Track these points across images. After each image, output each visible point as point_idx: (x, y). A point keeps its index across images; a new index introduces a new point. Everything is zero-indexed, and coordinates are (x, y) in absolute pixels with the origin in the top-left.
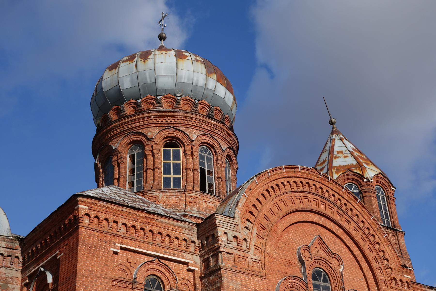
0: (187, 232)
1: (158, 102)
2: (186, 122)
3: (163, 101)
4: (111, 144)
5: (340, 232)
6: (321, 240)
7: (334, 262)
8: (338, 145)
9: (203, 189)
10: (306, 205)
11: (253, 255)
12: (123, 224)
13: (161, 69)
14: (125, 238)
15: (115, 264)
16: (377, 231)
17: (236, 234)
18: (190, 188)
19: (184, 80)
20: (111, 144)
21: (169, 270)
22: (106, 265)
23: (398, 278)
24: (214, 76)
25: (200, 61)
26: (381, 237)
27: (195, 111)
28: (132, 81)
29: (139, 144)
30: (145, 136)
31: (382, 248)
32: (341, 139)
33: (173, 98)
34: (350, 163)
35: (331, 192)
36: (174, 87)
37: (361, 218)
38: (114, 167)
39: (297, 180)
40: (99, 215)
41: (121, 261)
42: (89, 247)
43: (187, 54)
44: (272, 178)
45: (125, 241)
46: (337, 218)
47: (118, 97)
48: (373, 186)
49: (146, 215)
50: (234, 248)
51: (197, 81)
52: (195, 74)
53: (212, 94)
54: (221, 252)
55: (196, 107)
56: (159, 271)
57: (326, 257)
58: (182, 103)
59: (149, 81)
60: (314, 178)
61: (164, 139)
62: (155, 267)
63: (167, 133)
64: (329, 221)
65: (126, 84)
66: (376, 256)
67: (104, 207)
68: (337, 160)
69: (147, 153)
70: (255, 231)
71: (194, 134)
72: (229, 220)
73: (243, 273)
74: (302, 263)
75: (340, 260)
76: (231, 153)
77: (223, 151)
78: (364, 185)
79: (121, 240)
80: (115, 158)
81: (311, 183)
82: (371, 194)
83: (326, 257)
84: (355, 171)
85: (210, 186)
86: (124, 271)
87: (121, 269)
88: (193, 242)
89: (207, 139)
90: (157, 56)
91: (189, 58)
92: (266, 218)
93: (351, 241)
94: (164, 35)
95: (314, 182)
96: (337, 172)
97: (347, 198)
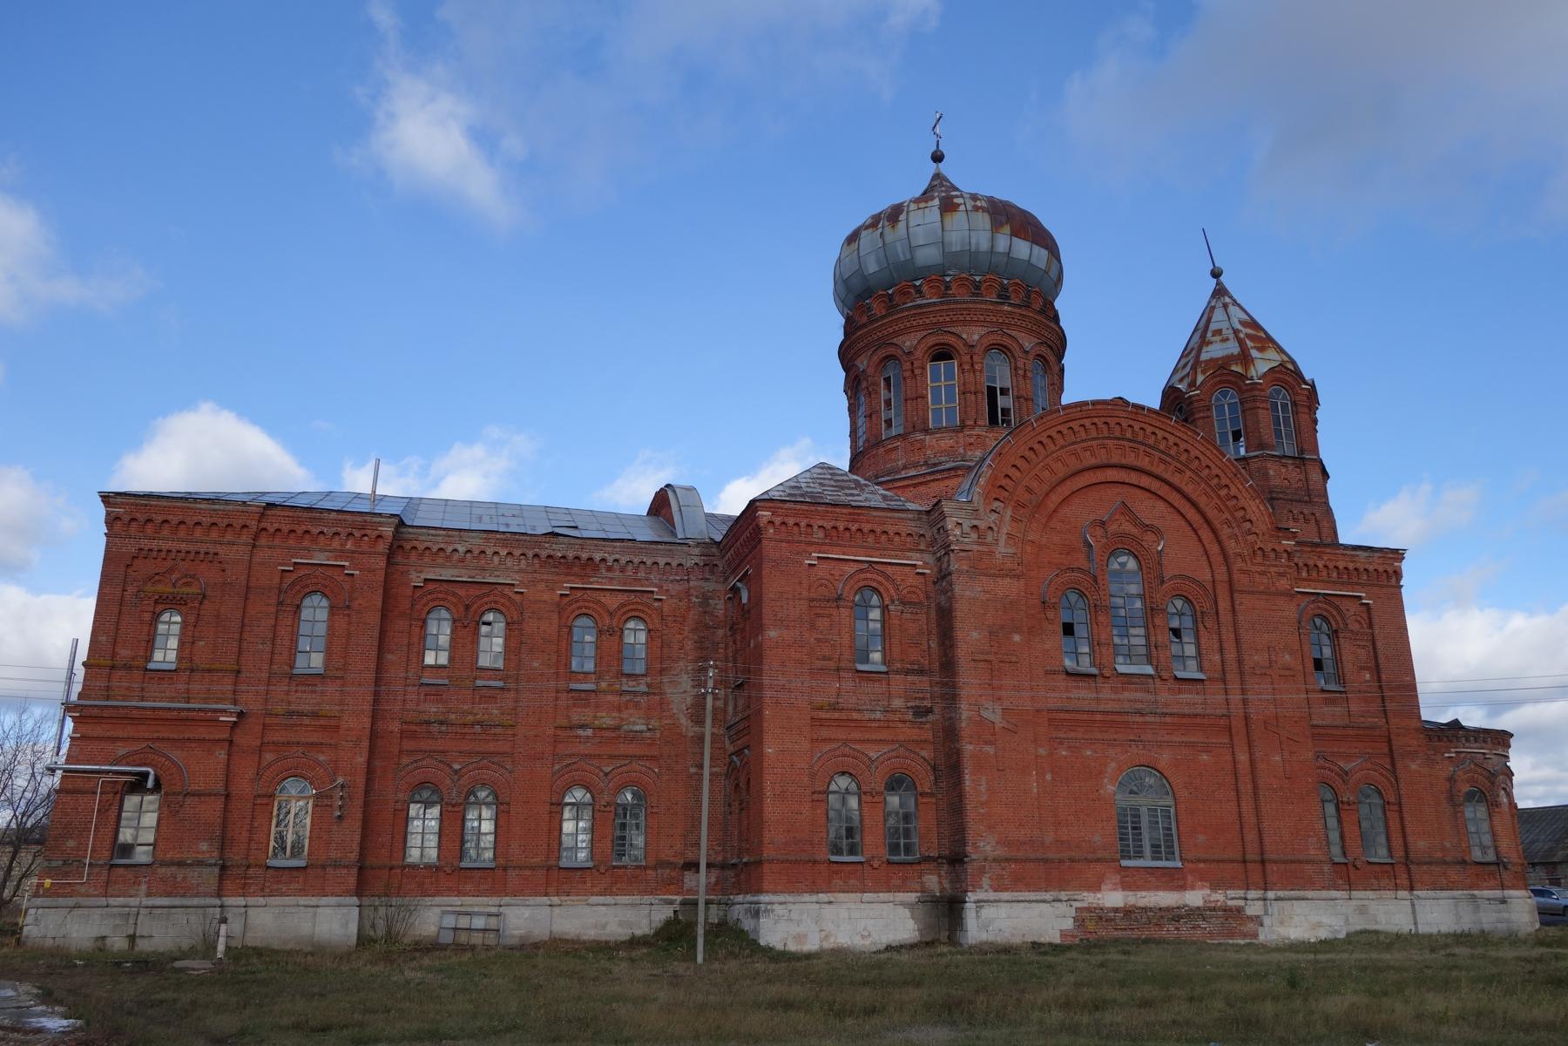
4: (500, 664)
5: (1164, 490)
6: (1125, 508)
7: (1150, 537)
9: (993, 420)
10: (1103, 458)
11: (1003, 549)
13: (919, 237)
17: (975, 522)
18: (971, 423)
19: (956, 248)
20: (500, 664)
21: (887, 577)
23: (1268, 548)
24: (1007, 229)
33: (936, 277)
34: (1229, 352)
35: (1149, 429)
37: (1205, 462)
39: (1087, 422)
46: (1159, 470)
51: (978, 244)
55: (978, 288)
57: (1134, 531)
63: (932, 340)
68: (1210, 348)
70: (1009, 513)
71: (974, 334)
75: (1158, 533)
76: (1044, 350)
77: (1027, 352)
81: (1112, 422)
83: (1134, 531)
84: (1234, 368)
85: (1005, 412)
91: (962, 208)
92: (1029, 490)
93: (1183, 501)
96: (1204, 372)
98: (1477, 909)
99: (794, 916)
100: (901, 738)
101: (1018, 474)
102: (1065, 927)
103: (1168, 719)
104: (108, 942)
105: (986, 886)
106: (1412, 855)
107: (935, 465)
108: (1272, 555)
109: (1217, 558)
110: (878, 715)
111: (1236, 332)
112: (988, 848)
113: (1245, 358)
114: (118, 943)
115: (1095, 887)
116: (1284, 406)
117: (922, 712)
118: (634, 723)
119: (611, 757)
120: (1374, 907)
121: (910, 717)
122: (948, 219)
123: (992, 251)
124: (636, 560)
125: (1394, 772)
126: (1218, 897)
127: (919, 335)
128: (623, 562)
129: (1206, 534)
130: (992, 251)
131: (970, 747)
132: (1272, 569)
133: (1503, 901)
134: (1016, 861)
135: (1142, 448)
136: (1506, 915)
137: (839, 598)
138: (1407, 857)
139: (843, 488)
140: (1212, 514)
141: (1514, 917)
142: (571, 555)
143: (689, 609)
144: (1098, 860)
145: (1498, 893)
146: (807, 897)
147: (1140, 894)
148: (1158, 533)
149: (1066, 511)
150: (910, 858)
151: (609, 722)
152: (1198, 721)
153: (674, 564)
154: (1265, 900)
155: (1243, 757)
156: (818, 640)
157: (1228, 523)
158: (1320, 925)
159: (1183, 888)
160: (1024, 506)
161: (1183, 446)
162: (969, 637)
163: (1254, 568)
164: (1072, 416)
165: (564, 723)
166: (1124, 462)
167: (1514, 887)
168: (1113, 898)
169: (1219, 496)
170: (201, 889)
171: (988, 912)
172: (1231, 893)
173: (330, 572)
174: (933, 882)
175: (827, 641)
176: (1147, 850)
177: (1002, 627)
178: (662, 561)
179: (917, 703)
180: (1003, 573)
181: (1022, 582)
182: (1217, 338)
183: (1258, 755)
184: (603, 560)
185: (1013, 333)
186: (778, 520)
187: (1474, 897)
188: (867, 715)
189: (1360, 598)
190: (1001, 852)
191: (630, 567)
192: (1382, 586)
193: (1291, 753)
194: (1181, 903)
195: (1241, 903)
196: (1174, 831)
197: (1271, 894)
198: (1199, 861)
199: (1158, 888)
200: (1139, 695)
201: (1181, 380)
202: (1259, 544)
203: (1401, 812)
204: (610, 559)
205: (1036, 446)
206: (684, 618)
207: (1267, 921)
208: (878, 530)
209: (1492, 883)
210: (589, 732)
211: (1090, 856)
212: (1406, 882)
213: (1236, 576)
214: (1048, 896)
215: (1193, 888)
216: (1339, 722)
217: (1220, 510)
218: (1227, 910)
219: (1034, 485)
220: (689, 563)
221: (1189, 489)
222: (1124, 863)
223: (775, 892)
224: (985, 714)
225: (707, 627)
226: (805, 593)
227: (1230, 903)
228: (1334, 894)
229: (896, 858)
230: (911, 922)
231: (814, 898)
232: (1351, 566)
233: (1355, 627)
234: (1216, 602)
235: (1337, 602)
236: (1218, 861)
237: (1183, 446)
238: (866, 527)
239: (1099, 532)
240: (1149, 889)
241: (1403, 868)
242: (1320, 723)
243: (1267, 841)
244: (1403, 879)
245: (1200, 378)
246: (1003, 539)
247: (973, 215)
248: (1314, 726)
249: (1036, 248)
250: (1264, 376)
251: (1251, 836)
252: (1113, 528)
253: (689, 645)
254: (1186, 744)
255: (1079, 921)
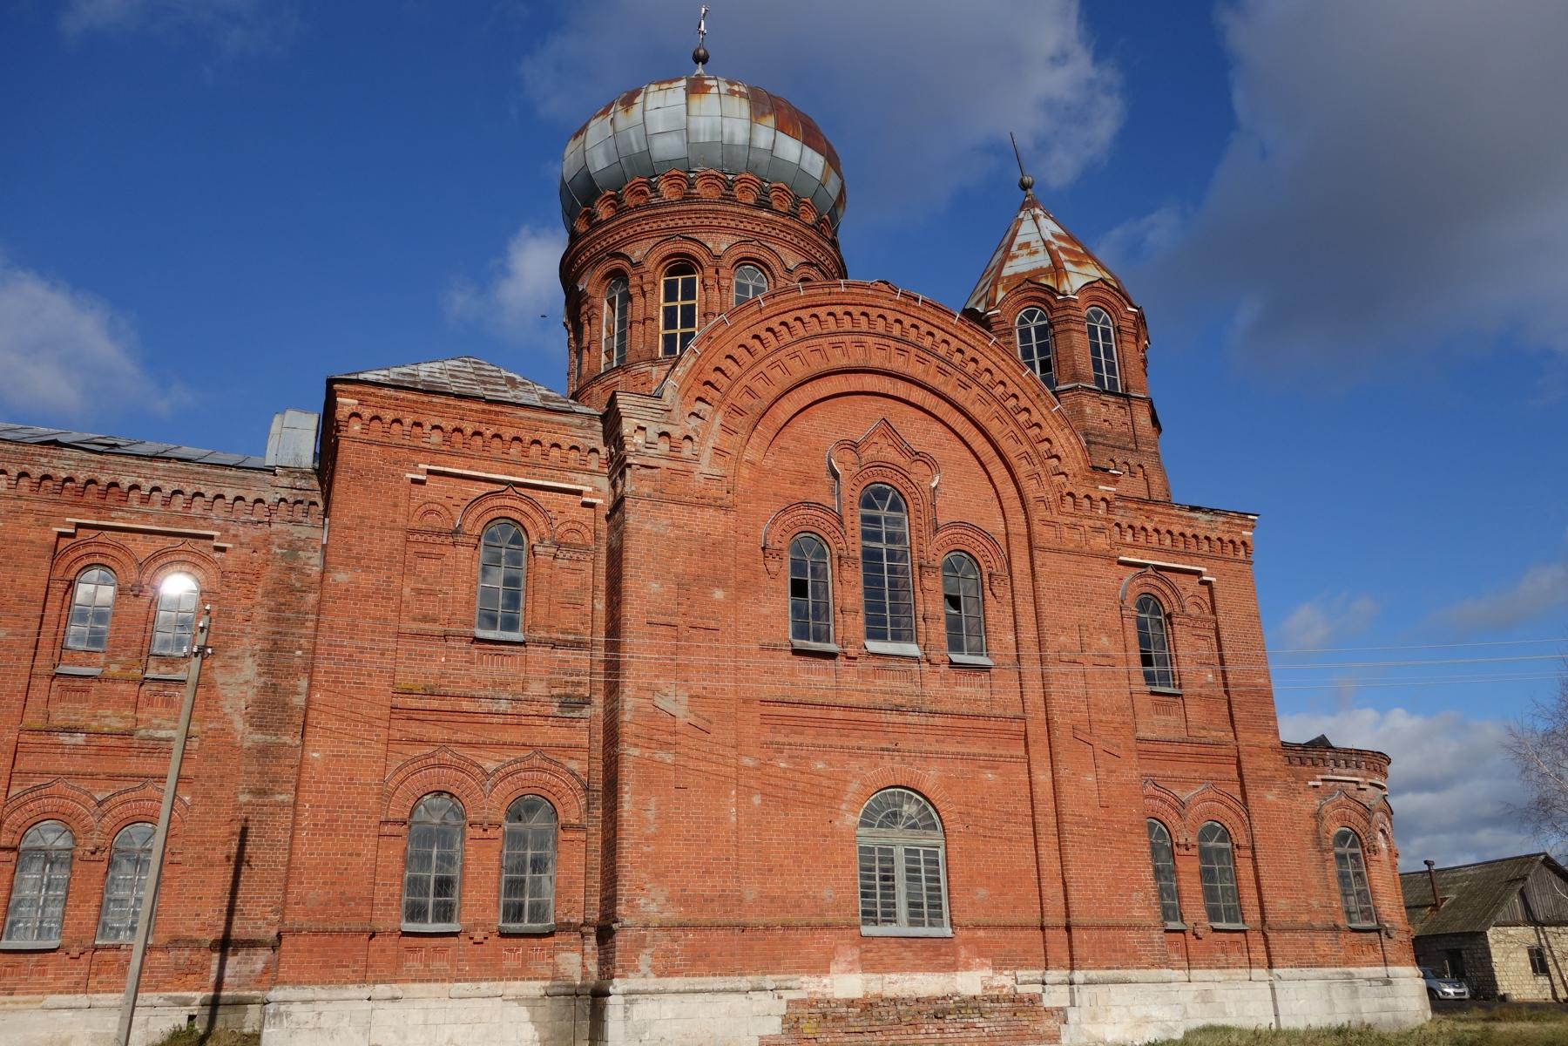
0: (580, 433)
1: (654, 189)
2: (706, 222)
3: (663, 186)
5: (942, 409)
6: (887, 428)
7: (919, 469)
8: (1027, 232)
12: (435, 427)
13: (658, 122)
14: (437, 452)
15: (416, 502)
16: (1037, 401)
17: (666, 428)
19: (704, 138)
21: (535, 506)
22: (395, 505)
23: (1080, 492)
24: (770, 121)
25: (740, 93)
26: (1045, 412)
27: (727, 198)
28: (607, 155)
29: (618, 276)
30: (627, 258)
31: (1047, 432)
32: (1035, 218)
33: (683, 174)
34: (1038, 265)
35: (924, 328)
36: (684, 155)
37: (999, 376)
39: (838, 310)
40: (381, 413)
41: (431, 495)
42: (359, 475)
43: (714, 83)
44: (767, 313)
45: (439, 457)
46: (937, 381)
48: (1079, 309)
49: (486, 407)
50: (661, 457)
51: (732, 134)
52: (726, 121)
53: (767, 158)
54: (629, 466)
55: (730, 188)
56: (1159, 589)
57: (902, 461)
58: (699, 184)
59: (637, 150)
60: (881, 302)
61: (664, 259)
62: (508, 502)
64: (915, 388)
65: (599, 162)
66: (1030, 451)
67: (390, 398)
68: (1015, 262)
69: (632, 291)
70: (719, 419)
71: (721, 243)
72: (650, 402)
73: (679, 503)
74: (836, 475)
75: (932, 464)
77: (790, 271)
78: (1058, 309)
79: (430, 457)
80: (584, 308)
81: (873, 312)
82: (1072, 326)
83: (902, 461)
84: (1043, 281)
86: (438, 513)
87: (431, 511)
88: (594, 450)
89: (751, 250)
90: (650, 96)
91: (714, 90)
92: (750, 392)
93: (969, 425)
94: (701, 52)
95: (881, 311)
97: (966, 338)
98: (1354, 993)
99: (326, 1022)
100: (539, 741)
101: (735, 368)
102: (767, 1032)
103: (938, 721)
105: (644, 968)
106: (1269, 919)
108: (1086, 503)
109: (1012, 503)
110: (504, 706)
111: (1046, 244)
112: (653, 908)
113: (1057, 270)
115: (821, 967)
116: (1106, 334)
117: (573, 702)
118: (159, 727)
119: (111, 777)
120: (1220, 992)
121: (555, 710)
122: (696, 101)
123: (750, 146)
124: (189, 490)
125: (1245, 804)
126: (1005, 981)
127: (652, 242)
128: (168, 490)
129: (998, 470)
130: (750, 146)
131: (636, 752)
132: (1086, 522)
133: (1387, 982)
134: (696, 927)
135: (914, 350)
136: (1390, 1001)
137: (456, 532)
138: (1263, 920)
139: (484, 382)
140: (1007, 446)
141: (1402, 1003)
142: (82, 476)
143: (266, 563)
144: (827, 926)
145: (1380, 971)
146: (353, 991)
147: (888, 977)
148: (932, 464)
149: (800, 424)
150: (538, 926)
151: (116, 724)
152: (981, 723)
153: (250, 498)
154: (1071, 983)
155: (1043, 777)
156: (418, 591)
157: (1026, 456)
158: (1147, 1020)
159: (953, 967)
160: (741, 413)
161: (969, 353)
162: (646, 589)
163: (1061, 519)
164: (818, 300)
165: (39, 724)
166: (888, 366)
167: (1397, 963)
168: (846, 984)
169: (1016, 423)
171: (644, 1010)
172: (1023, 974)
174: (576, 963)
175: (432, 593)
176: (902, 910)
177: (698, 578)
178: (230, 494)
179: (569, 690)
180: (701, 503)
181: (732, 516)
182: (1025, 251)
183: (1063, 773)
184: (135, 487)
185: (774, 247)
186: (367, 413)
187: (1350, 976)
188: (486, 706)
189: (1199, 574)
190: (673, 914)
191: (179, 499)
192: (1227, 560)
193: (1109, 772)
194: (949, 990)
195: (1038, 989)
196: (943, 884)
197: (1079, 976)
198: (977, 927)
199: (915, 968)
200: (898, 684)
201: (978, 303)
202: (1069, 488)
203: (1254, 859)
204: (147, 487)
205: (764, 335)
206: (258, 575)
207: (1073, 1015)
208: (527, 438)
209: (1372, 956)
210: (80, 738)
211: (814, 920)
212: (1263, 957)
213: (1037, 527)
214: (744, 983)
215: (967, 967)
216: (1172, 736)
217: (1018, 441)
218: (1015, 999)
219: (759, 386)
220: (270, 497)
221: (976, 410)
222: (867, 930)
223: (298, 983)
224: (662, 703)
225: (291, 590)
226: (401, 521)
227: (1021, 989)
228: (1166, 973)
229: (513, 926)
230: (530, 1027)
231: (366, 991)
232: (1189, 532)
233: (1195, 611)
234: (1009, 562)
235: (1171, 576)
236: (1005, 927)
237: (969, 353)
238: (508, 433)
239: (849, 456)
240: (903, 970)
241: (1259, 937)
242: (1149, 735)
243: (1074, 896)
244: (1259, 953)
245: (1001, 295)
246: (707, 455)
247: (728, 100)
248: (1139, 740)
249: (808, 151)
250: (1080, 291)
251: (1053, 890)
252: (869, 453)
253: (260, 614)
254: (963, 757)
255: (791, 1023)
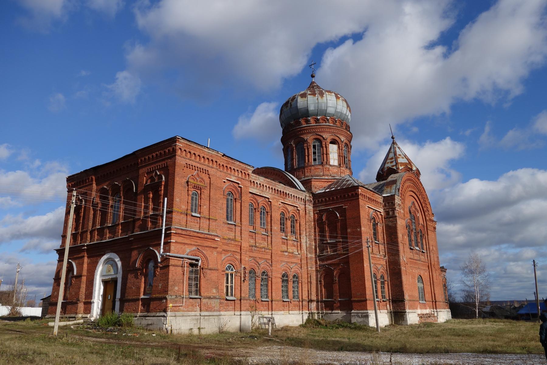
19: (339, 110)
28: (315, 107)
38: (305, 149)
47: (306, 114)
65: (312, 108)
80: (305, 145)
104: (193, 330)
107: (333, 177)
114: (196, 332)
170: (216, 308)
173: (235, 184)
